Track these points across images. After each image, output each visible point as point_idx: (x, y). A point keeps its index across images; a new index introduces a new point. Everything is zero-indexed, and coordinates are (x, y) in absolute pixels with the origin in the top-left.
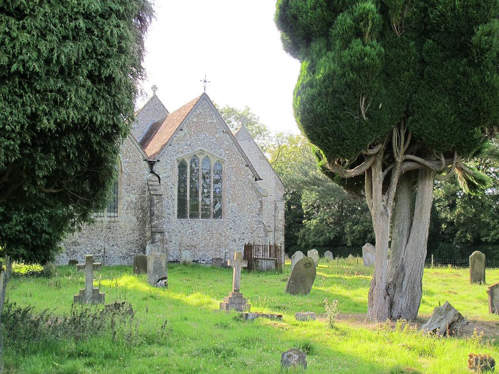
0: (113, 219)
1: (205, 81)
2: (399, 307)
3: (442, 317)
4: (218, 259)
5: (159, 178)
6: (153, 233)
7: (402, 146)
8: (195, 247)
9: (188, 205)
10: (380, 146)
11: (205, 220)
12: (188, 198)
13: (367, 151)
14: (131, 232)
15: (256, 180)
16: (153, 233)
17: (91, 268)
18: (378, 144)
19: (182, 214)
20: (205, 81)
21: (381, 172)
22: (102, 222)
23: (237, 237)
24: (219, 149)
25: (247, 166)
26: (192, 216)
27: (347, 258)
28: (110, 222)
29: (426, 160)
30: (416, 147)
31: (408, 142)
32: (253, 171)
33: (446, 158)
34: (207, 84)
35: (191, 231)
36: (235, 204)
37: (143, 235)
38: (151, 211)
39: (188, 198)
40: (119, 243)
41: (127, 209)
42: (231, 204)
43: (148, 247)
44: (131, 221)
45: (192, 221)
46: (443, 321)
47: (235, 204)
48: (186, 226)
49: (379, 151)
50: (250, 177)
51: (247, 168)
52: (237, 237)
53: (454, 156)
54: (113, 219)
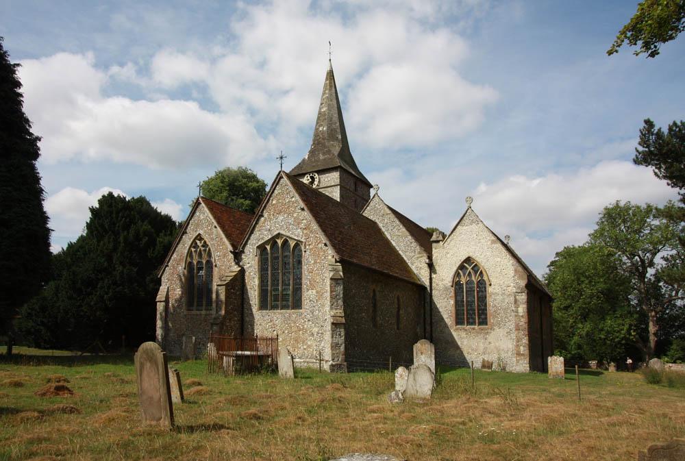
22: (201, 314)
23: (315, 330)
36: (314, 291)
47: (314, 291)
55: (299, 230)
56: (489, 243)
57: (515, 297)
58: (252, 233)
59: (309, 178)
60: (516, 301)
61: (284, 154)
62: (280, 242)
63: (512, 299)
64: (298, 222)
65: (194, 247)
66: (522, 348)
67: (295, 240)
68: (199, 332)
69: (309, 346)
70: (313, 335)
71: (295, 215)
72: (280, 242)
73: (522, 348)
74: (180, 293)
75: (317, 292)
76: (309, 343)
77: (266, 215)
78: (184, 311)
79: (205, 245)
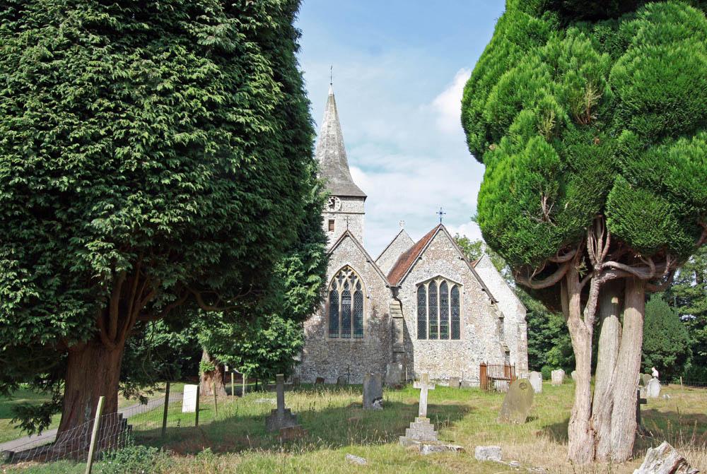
0: (358, 340)
1: (441, 213)
2: (606, 444)
3: (659, 462)
4: (455, 378)
5: (400, 302)
6: (395, 353)
7: (599, 251)
8: (435, 366)
9: (428, 327)
10: (573, 253)
11: (444, 341)
12: (428, 321)
13: (556, 259)
14: (376, 351)
15: (492, 303)
16: (395, 353)
17: (282, 388)
18: (571, 249)
19: (421, 335)
20: (441, 213)
21: (578, 283)
22: (349, 342)
23: (475, 356)
24: (456, 274)
25: (483, 290)
26: (431, 337)
27: (216, 419)
28: (356, 342)
29: (632, 267)
30: (619, 253)
31: (607, 247)
32: (489, 294)
33: (656, 263)
34: (443, 216)
35: (431, 351)
36: (473, 326)
37: (385, 355)
38: (392, 332)
39: (428, 321)
40: (365, 362)
41: (372, 331)
42: (469, 326)
43: (388, 366)
44: (375, 342)
45: (432, 342)
46: (660, 467)
47: (473, 326)
48: (427, 346)
49: (573, 258)
50: (487, 300)
51: (483, 292)
52: (475, 356)
53: (666, 261)
54: (358, 340)
55: (458, 275)
56: (500, 283)
57: (518, 326)
58: (410, 272)
59: (330, 201)
60: (519, 330)
61: (444, 211)
62: (438, 283)
63: (516, 327)
64: (457, 269)
65: (338, 277)
66: (523, 365)
67: (455, 282)
68: (346, 358)
69: (470, 369)
70: (473, 360)
71: (454, 262)
72: (438, 283)
73: (523, 365)
74: (319, 320)
75: (476, 326)
76: (470, 367)
77: (424, 257)
78: (326, 337)
79: (353, 277)
